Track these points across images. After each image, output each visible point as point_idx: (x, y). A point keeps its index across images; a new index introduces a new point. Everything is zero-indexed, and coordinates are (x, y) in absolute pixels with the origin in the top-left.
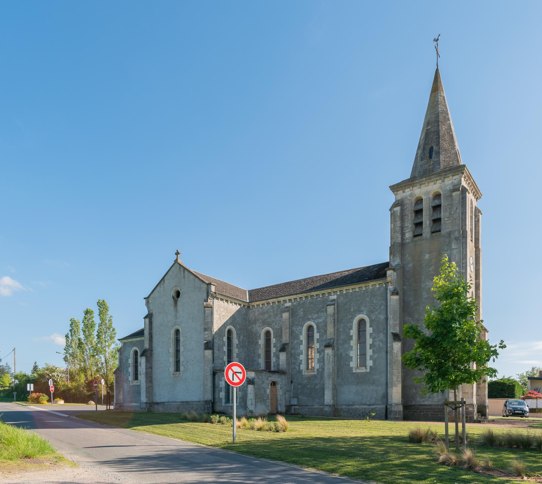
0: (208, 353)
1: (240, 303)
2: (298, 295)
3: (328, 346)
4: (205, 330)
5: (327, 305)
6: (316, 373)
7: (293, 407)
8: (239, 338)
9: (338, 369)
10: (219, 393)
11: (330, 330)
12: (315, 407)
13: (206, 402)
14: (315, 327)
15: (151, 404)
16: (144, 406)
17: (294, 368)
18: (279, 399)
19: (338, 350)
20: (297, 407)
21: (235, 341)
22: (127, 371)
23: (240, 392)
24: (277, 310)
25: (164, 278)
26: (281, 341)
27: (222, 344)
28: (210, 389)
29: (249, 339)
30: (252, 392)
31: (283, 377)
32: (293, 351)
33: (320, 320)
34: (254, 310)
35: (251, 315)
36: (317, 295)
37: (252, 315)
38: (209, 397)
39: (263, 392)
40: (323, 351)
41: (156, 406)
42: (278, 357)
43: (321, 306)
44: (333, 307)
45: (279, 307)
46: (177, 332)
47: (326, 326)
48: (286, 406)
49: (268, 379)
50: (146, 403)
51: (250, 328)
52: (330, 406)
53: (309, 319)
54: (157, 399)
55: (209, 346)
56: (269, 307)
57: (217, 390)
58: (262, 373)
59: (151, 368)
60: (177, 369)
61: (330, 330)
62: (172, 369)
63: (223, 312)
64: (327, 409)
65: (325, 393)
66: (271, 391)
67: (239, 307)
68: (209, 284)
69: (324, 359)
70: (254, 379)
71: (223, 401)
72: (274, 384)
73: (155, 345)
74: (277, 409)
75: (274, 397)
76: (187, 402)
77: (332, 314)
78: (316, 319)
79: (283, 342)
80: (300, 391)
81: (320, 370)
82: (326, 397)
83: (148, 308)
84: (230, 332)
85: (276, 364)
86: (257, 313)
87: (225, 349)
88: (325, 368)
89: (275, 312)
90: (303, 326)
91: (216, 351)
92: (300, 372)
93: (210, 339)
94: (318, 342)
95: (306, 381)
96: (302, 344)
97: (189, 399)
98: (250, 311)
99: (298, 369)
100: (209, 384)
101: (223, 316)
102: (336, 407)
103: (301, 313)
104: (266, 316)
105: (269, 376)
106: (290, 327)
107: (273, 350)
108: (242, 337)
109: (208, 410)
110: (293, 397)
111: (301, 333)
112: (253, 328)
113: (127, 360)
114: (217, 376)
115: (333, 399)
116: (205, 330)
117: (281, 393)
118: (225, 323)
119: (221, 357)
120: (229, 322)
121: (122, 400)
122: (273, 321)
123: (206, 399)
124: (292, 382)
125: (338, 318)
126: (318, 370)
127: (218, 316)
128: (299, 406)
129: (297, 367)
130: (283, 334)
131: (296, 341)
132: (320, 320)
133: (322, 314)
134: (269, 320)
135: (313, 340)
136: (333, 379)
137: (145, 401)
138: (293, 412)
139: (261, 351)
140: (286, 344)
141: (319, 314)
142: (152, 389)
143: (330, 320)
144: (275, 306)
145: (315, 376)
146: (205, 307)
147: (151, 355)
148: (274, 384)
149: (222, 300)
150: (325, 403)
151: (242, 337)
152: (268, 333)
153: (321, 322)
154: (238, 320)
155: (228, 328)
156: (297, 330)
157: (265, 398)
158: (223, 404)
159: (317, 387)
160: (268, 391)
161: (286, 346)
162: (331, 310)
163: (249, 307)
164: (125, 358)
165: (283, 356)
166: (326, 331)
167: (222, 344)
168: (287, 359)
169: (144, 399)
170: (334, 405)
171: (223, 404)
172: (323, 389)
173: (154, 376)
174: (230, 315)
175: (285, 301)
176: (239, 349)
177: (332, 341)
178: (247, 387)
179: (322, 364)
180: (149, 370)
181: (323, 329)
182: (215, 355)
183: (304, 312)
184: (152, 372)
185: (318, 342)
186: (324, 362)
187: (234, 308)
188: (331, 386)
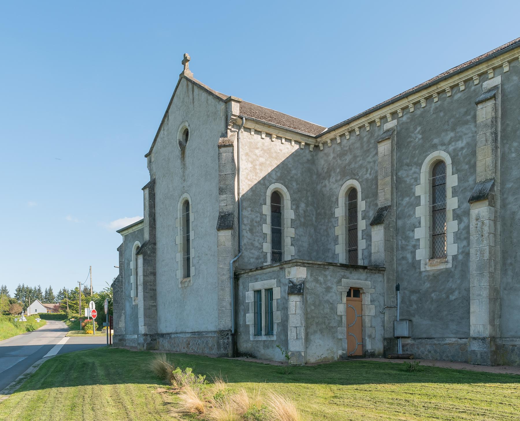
0: (226, 235)
1: (298, 138)
2: (411, 98)
3: (477, 198)
4: (221, 191)
5: (477, 103)
6: (450, 265)
7: (400, 342)
8: (298, 207)
9: (504, 253)
10: (245, 316)
11: (485, 160)
12: (448, 341)
13: (221, 333)
14: (448, 161)
15: (154, 339)
16: (141, 340)
17: (404, 258)
18: (368, 323)
19: (504, 206)
20: (409, 341)
21: (289, 214)
22: (129, 282)
23: (279, 313)
24: (369, 141)
25: (167, 112)
26: (376, 205)
27: (258, 219)
28: (228, 307)
29: (317, 208)
30: (299, 311)
31: (378, 277)
32: (400, 223)
33: (460, 144)
34: (326, 151)
35: (322, 163)
36: (452, 88)
37: (322, 162)
38: (227, 323)
39: (327, 310)
40: (467, 213)
41: (161, 339)
42: (368, 237)
43: (463, 110)
44: (490, 104)
45: (371, 133)
46: (187, 204)
47: (474, 154)
48: (385, 339)
49: (339, 282)
50: (145, 335)
51: (319, 187)
52: (483, 339)
53: (434, 147)
54: (163, 328)
55: (225, 222)
56: (353, 138)
57: (241, 308)
58: (325, 269)
59: (154, 274)
60: (188, 275)
61: (485, 160)
62: (180, 273)
63: (257, 158)
64: (475, 347)
65: (472, 310)
66: (348, 309)
67: (297, 147)
68: (229, 101)
69: (468, 233)
70: (304, 283)
71: (252, 330)
72: (355, 293)
73: (158, 235)
74: (363, 346)
75: (356, 324)
76: (199, 333)
77: (489, 122)
78: (449, 143)
79: (380, 206)
80: (415, 306)
81: (460, 257)
82: (473, 320)
83: (150, 170)
84: (276, 197)
85: (366, 253)
86: (332, 156)
87: (267, 229)
88: (472, 251)
89: (365, 148)
90: (420, 165)
91: (246, 235)
92: (415, 265)
93: (229, 208)
94: (455, 193)
95: (427, 285)
96: (419, 204)
97: (202, 328)
98: (321, 154)
99: (410, 261)
100: (228, 298)
101: (261, 164)
102: (499, 342)
103: (417, 137)
104: (348, 158)
105: (344, 277)
106: (395, 172)
107: (362, 224)
108: (303, 205)
109: (225, 348)
110: (401, 320)
111: (417, 180)
112: (325, 186)
113: (129, 264)
114: (241, 281)
115: (492, 322)
116: (221, 191)
117: (373, 312)
118: (264, 179)
119: (257, 244)
120: (274, 176)
121: (123, 329)
122: (361, 167)
123: (222, 327)
124: (398, 288)
125: (503, 130)
126: (455, 258)
127: (250, 165)
128: (414, 339)
129: (409, 256)
130: (380, 187)
131: (407, 199)
132: (460, 144)
133: (464, 129)
134: (353, 166)
135: (444, 191)
136: (492, 276)
137: (143, 332)
138: (400, 352)
139: (340, 231)
140: (386, 208)
141: (458, 129)
142: (156, 310)
143: (484, 138)
144: (364, 134)
145: (448, 273)
146: (220, 147)
147: (154, 251)
148: (355, 293)
149: (258, 132)
150: (472, 333)
151: (303, 205)
152: (352, 193)
153: (462, 148)
154: (294, 172)
155: (272, 187)
156: (408, 176)
157: (333, 324)
158: (252, 338)
159: (452, 297)
160: (341, 309)
161: (385, 213)
162: (485, 112)
163: (317, 147)
164: (126, 261)
165: (378, 234)
166: (474, 167)
167: (258, 219)
168: (387, 240)
169: (142, 329)
170: (493, 338)
171: (252, 338)
172: (466, 301)
173: (159, 288)
174: (276, 163)
175: (383, 118)
176: (296, 228)
177: (489, 185)
178: (287, 300)
179: (465, 243)
180: (151, 278)
181: (466, 162)
182: (244, 241)
183: (423, 133)
184: (155, 281)
185: (455, 193)
186: (468, 238)
187: (285, 149)
188: (485, 293)
